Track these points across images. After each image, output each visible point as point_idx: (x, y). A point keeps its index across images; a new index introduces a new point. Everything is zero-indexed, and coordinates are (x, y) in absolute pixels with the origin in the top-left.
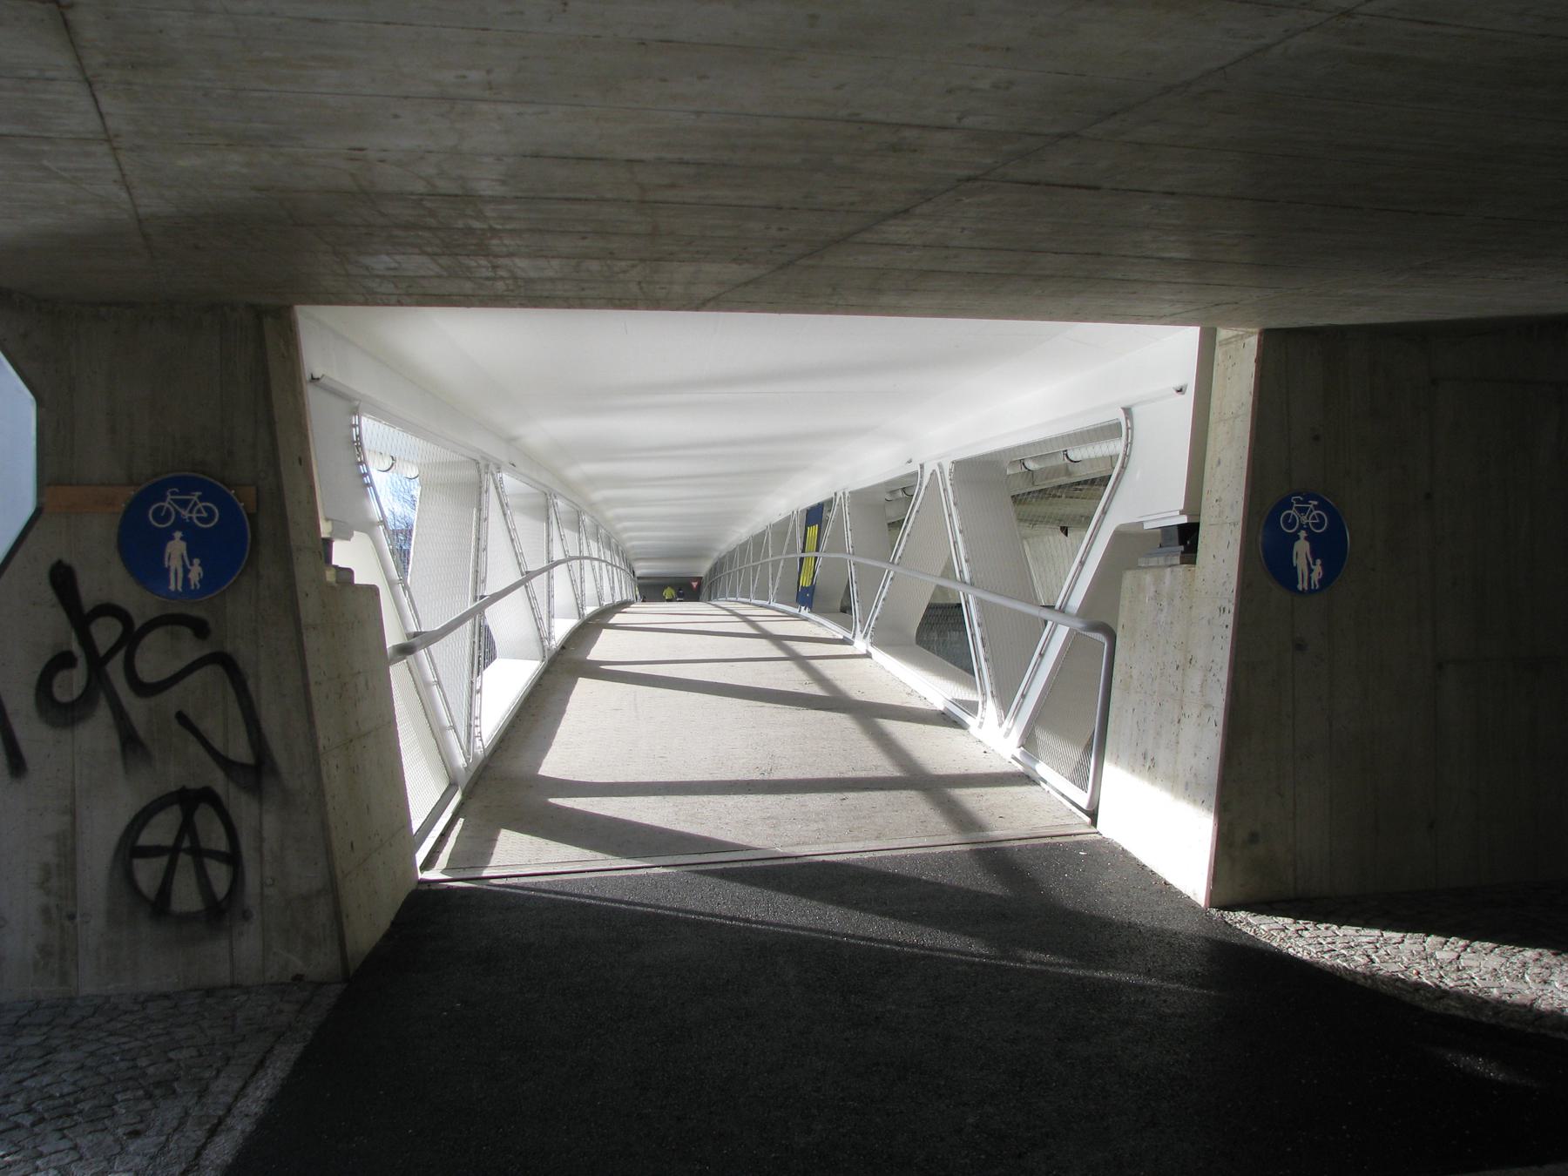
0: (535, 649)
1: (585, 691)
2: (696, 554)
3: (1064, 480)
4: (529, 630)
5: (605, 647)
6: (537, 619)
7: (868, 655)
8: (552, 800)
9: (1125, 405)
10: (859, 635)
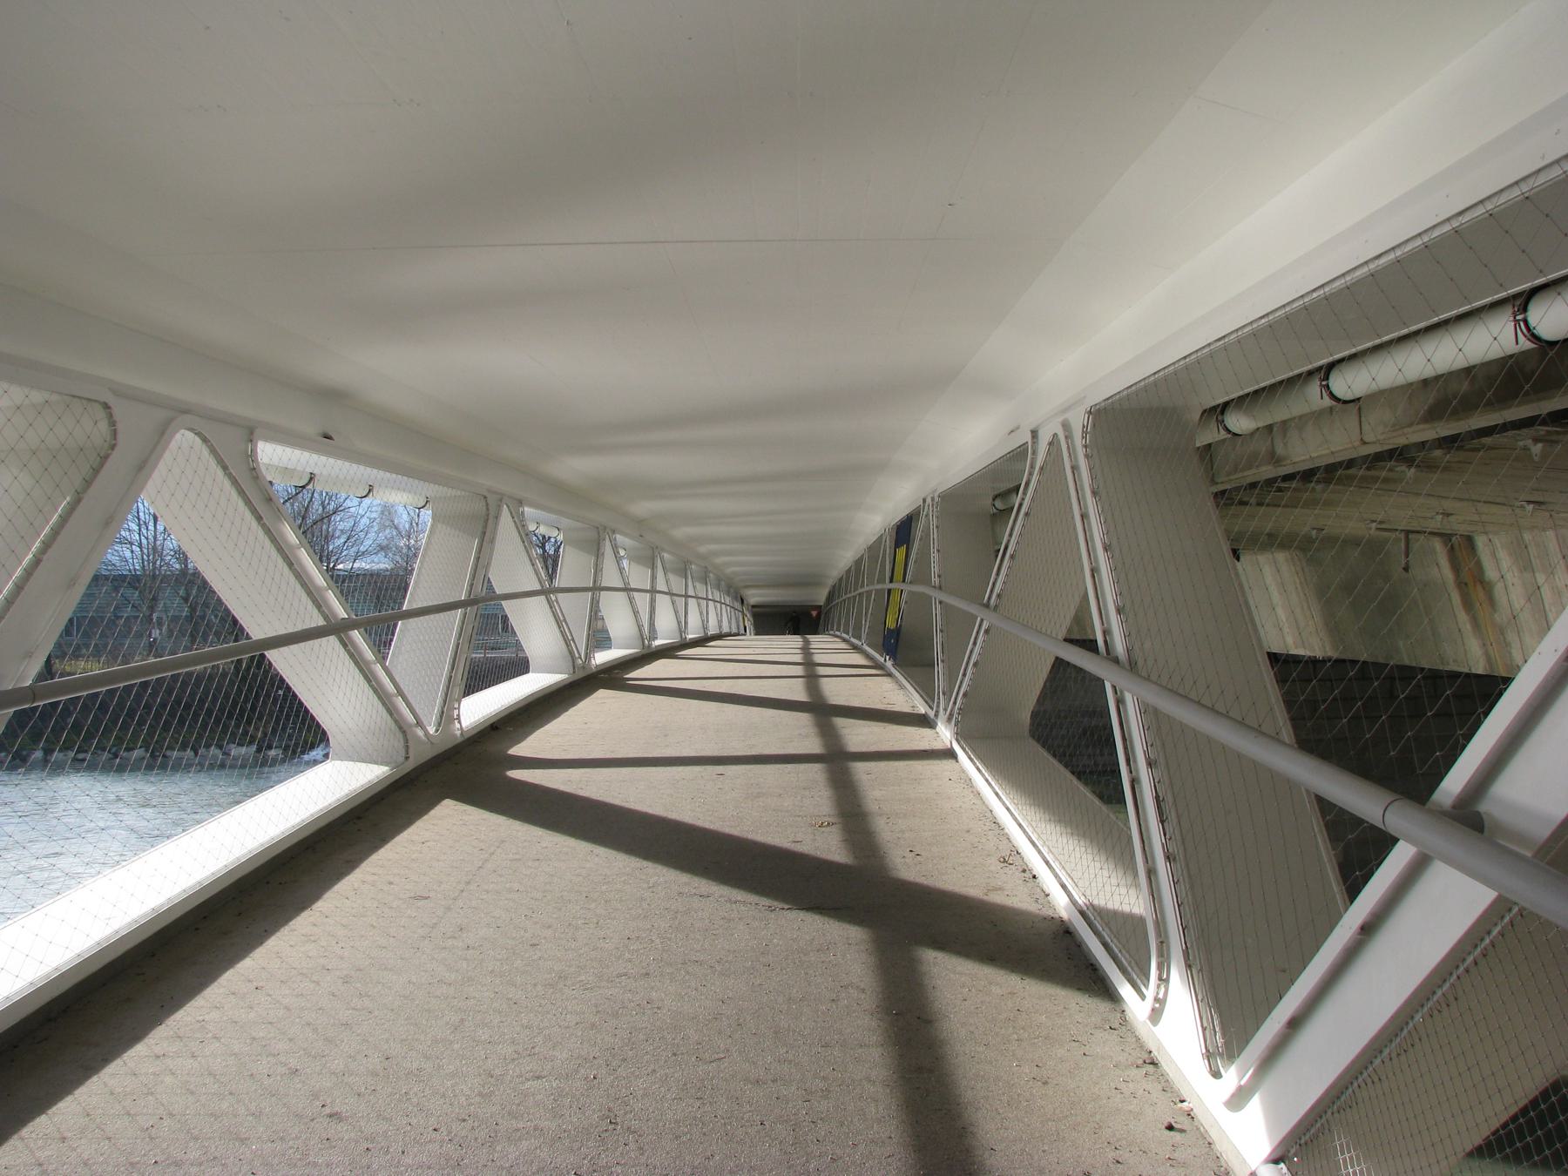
2: (808, 581)
3: (1266, 472)
7: (950, 754)
10: (943, 716)
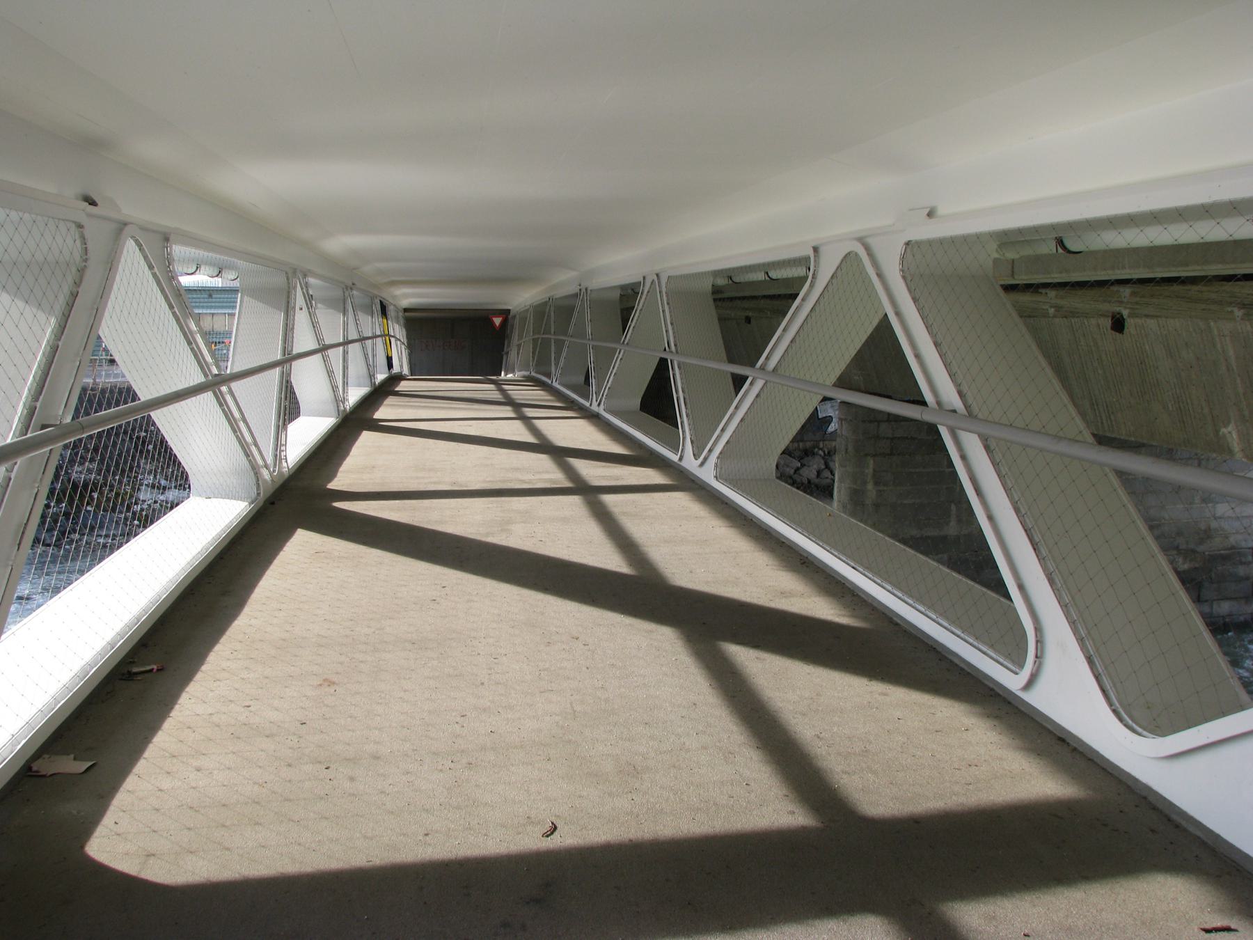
0: (331, 407)
1: (367, 438)
4: (327, 394)
5: (384, 412)
6: (334, 388)
8: (337, 504)
9: (814, 244)
